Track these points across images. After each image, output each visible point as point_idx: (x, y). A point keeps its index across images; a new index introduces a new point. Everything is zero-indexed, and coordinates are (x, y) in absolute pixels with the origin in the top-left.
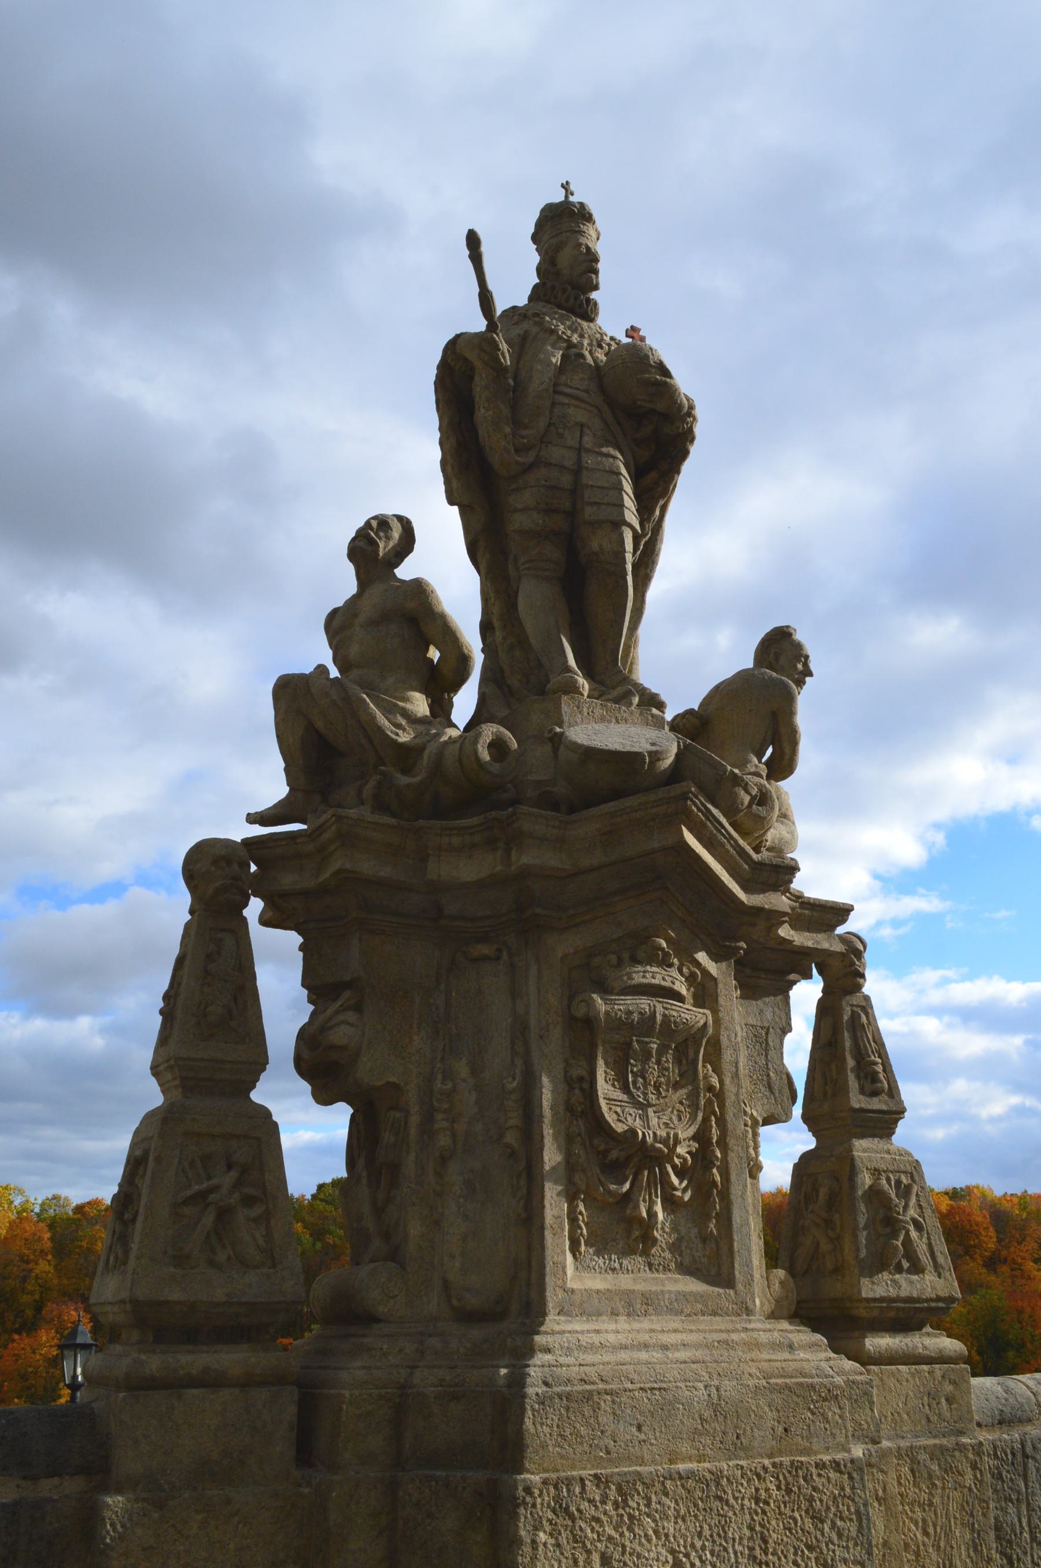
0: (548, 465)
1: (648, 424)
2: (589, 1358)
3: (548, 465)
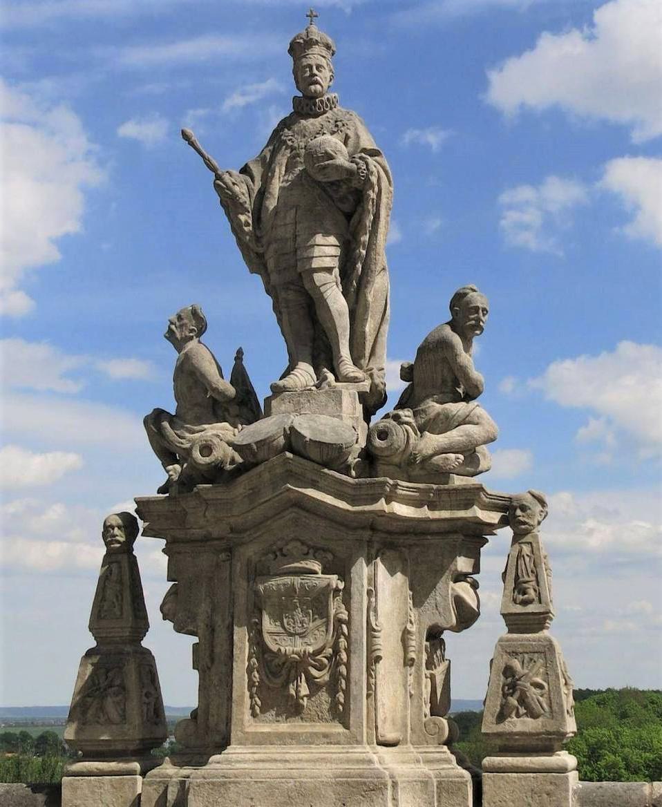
0: (276, 241)
1: (342, 200)
2: (238, 766)
3: (276, 241)
